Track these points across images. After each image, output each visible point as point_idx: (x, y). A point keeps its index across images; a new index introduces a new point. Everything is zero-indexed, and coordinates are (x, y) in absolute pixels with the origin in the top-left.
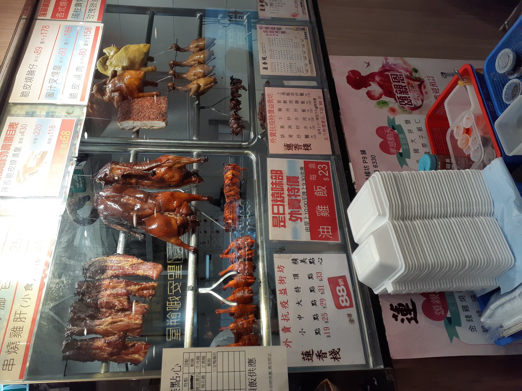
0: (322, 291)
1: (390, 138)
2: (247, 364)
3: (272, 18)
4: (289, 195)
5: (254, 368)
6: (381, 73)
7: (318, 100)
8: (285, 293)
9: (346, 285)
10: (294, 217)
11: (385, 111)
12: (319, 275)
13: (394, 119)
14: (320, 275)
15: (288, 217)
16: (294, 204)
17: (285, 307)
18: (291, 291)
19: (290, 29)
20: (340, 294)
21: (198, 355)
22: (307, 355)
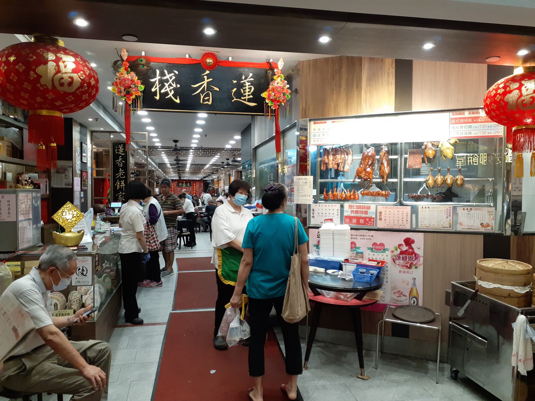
1: (379, 247)
6: (413, 253)
10: (352, 212)
14: (334, 216)
16: (357, 212)
18: (329, 208)
22: (313, 210)
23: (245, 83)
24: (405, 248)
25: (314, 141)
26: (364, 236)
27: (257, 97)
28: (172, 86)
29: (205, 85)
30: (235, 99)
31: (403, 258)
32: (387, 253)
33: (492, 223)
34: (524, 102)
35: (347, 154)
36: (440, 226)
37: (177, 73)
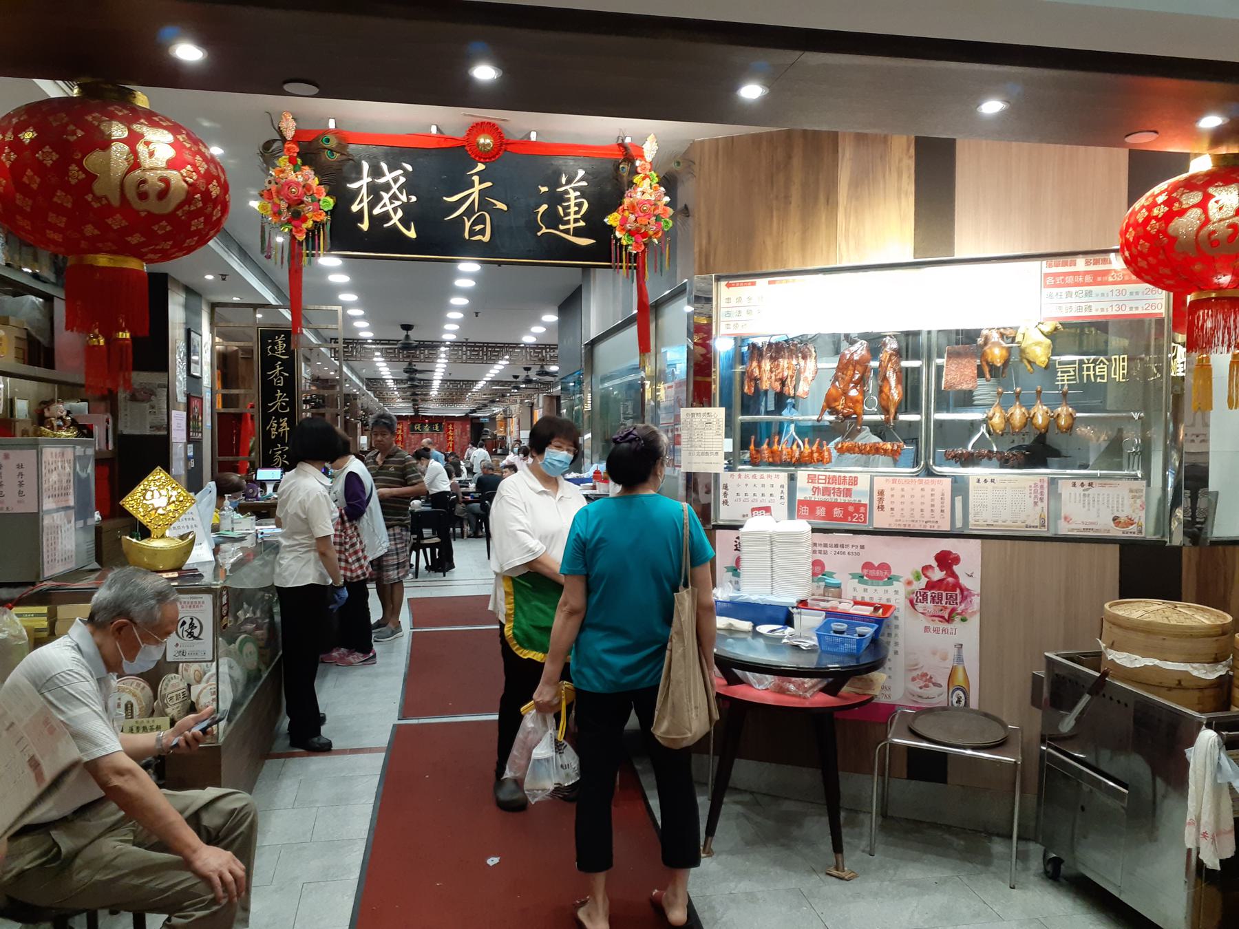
1: (878, 573)
6: (957, 585)
10: (816, 490)
14: (773, 501)
16: (826, 491)
18: (762, 482)
22: (726, 487)
23: (566, 192)
24: (937, 575)
25: (728, 326)
26: (842, 546)
27: (594, 225)
28: (398, 199)
29: (476, 196)
30: (544, 230)
31: (933, 598)
32: (897, 585)
33: (1139, 516)
34: (1213, 237)
35: (804, 358)
36: (1019, 523)
37: (409, 168)
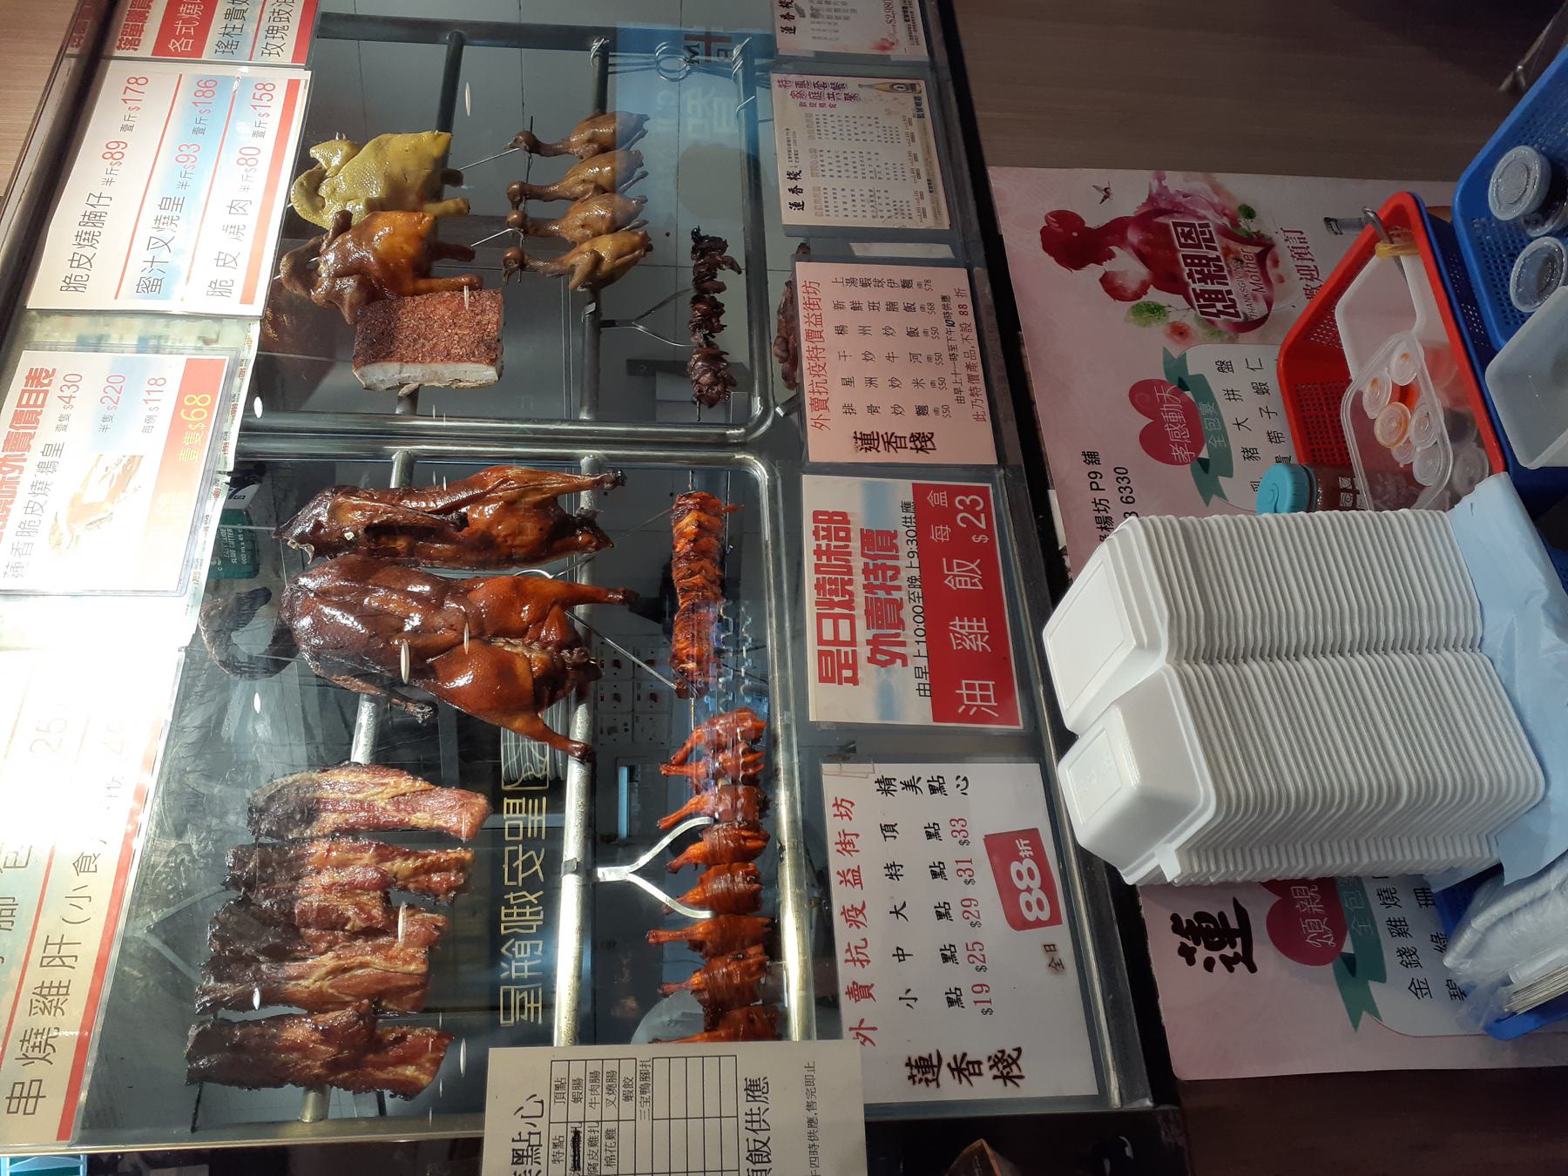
0: (966, 877)
1: (1172, 416)
2: (742, 1094)
3: (817, 53)
4: (868, 588)
5: (763, 1106)
6: (1144, 220)
7: (955, 302)
8: (857, 881)
9: (1039, 857)
10: (884, 653)
11: (1157, 334)
12: (958, 827)
13: (1183, 359)
14: (960, 827)
15: (864, 651)
16: (883, 614)
17: (857, 924)
18: (873, 875)
19: (870, 86)
20: (1020, 885)
21: (593, 1067)
22: (924, 1068)
